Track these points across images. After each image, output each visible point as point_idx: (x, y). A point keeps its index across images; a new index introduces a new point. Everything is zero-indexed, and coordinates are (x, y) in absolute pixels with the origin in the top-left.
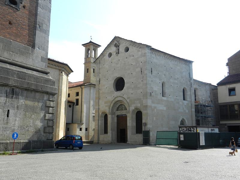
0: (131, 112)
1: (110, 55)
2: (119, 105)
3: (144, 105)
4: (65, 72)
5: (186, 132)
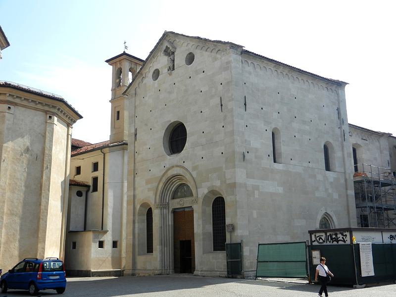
0: (200, 201)
1: (156, 74)
2: (178, 187)
3: (228, 182)
4: (59, 117)
5: (325, 244)
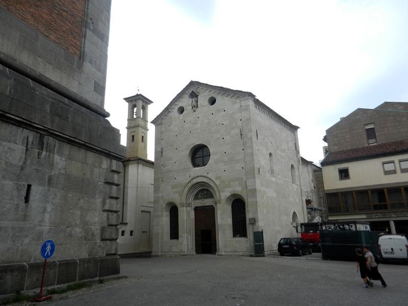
2: (203, 190)
3: (249, 188)
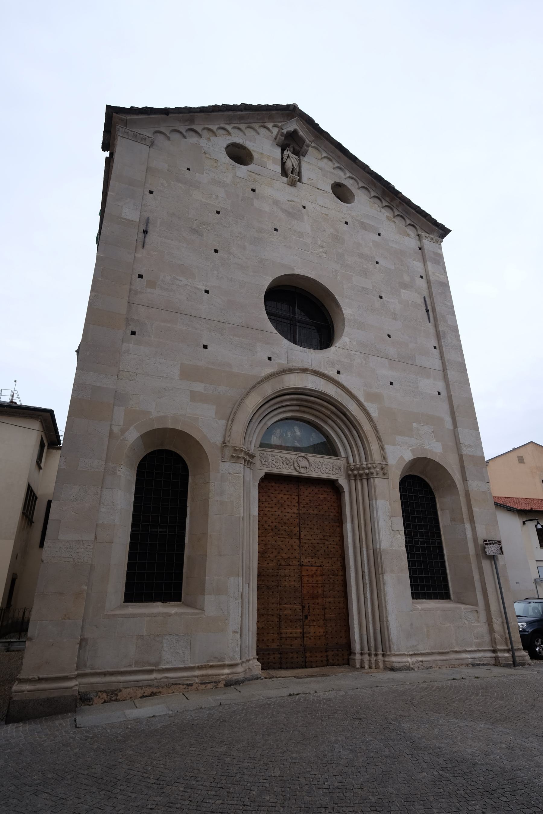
2: (319, 416)
